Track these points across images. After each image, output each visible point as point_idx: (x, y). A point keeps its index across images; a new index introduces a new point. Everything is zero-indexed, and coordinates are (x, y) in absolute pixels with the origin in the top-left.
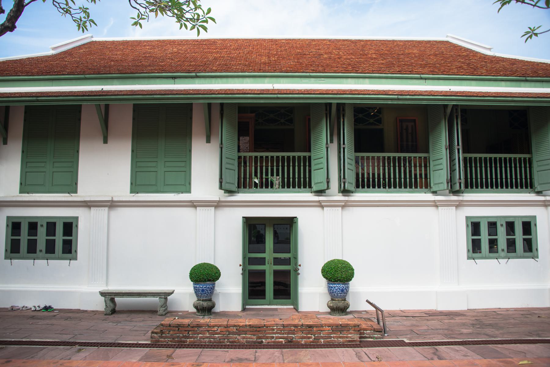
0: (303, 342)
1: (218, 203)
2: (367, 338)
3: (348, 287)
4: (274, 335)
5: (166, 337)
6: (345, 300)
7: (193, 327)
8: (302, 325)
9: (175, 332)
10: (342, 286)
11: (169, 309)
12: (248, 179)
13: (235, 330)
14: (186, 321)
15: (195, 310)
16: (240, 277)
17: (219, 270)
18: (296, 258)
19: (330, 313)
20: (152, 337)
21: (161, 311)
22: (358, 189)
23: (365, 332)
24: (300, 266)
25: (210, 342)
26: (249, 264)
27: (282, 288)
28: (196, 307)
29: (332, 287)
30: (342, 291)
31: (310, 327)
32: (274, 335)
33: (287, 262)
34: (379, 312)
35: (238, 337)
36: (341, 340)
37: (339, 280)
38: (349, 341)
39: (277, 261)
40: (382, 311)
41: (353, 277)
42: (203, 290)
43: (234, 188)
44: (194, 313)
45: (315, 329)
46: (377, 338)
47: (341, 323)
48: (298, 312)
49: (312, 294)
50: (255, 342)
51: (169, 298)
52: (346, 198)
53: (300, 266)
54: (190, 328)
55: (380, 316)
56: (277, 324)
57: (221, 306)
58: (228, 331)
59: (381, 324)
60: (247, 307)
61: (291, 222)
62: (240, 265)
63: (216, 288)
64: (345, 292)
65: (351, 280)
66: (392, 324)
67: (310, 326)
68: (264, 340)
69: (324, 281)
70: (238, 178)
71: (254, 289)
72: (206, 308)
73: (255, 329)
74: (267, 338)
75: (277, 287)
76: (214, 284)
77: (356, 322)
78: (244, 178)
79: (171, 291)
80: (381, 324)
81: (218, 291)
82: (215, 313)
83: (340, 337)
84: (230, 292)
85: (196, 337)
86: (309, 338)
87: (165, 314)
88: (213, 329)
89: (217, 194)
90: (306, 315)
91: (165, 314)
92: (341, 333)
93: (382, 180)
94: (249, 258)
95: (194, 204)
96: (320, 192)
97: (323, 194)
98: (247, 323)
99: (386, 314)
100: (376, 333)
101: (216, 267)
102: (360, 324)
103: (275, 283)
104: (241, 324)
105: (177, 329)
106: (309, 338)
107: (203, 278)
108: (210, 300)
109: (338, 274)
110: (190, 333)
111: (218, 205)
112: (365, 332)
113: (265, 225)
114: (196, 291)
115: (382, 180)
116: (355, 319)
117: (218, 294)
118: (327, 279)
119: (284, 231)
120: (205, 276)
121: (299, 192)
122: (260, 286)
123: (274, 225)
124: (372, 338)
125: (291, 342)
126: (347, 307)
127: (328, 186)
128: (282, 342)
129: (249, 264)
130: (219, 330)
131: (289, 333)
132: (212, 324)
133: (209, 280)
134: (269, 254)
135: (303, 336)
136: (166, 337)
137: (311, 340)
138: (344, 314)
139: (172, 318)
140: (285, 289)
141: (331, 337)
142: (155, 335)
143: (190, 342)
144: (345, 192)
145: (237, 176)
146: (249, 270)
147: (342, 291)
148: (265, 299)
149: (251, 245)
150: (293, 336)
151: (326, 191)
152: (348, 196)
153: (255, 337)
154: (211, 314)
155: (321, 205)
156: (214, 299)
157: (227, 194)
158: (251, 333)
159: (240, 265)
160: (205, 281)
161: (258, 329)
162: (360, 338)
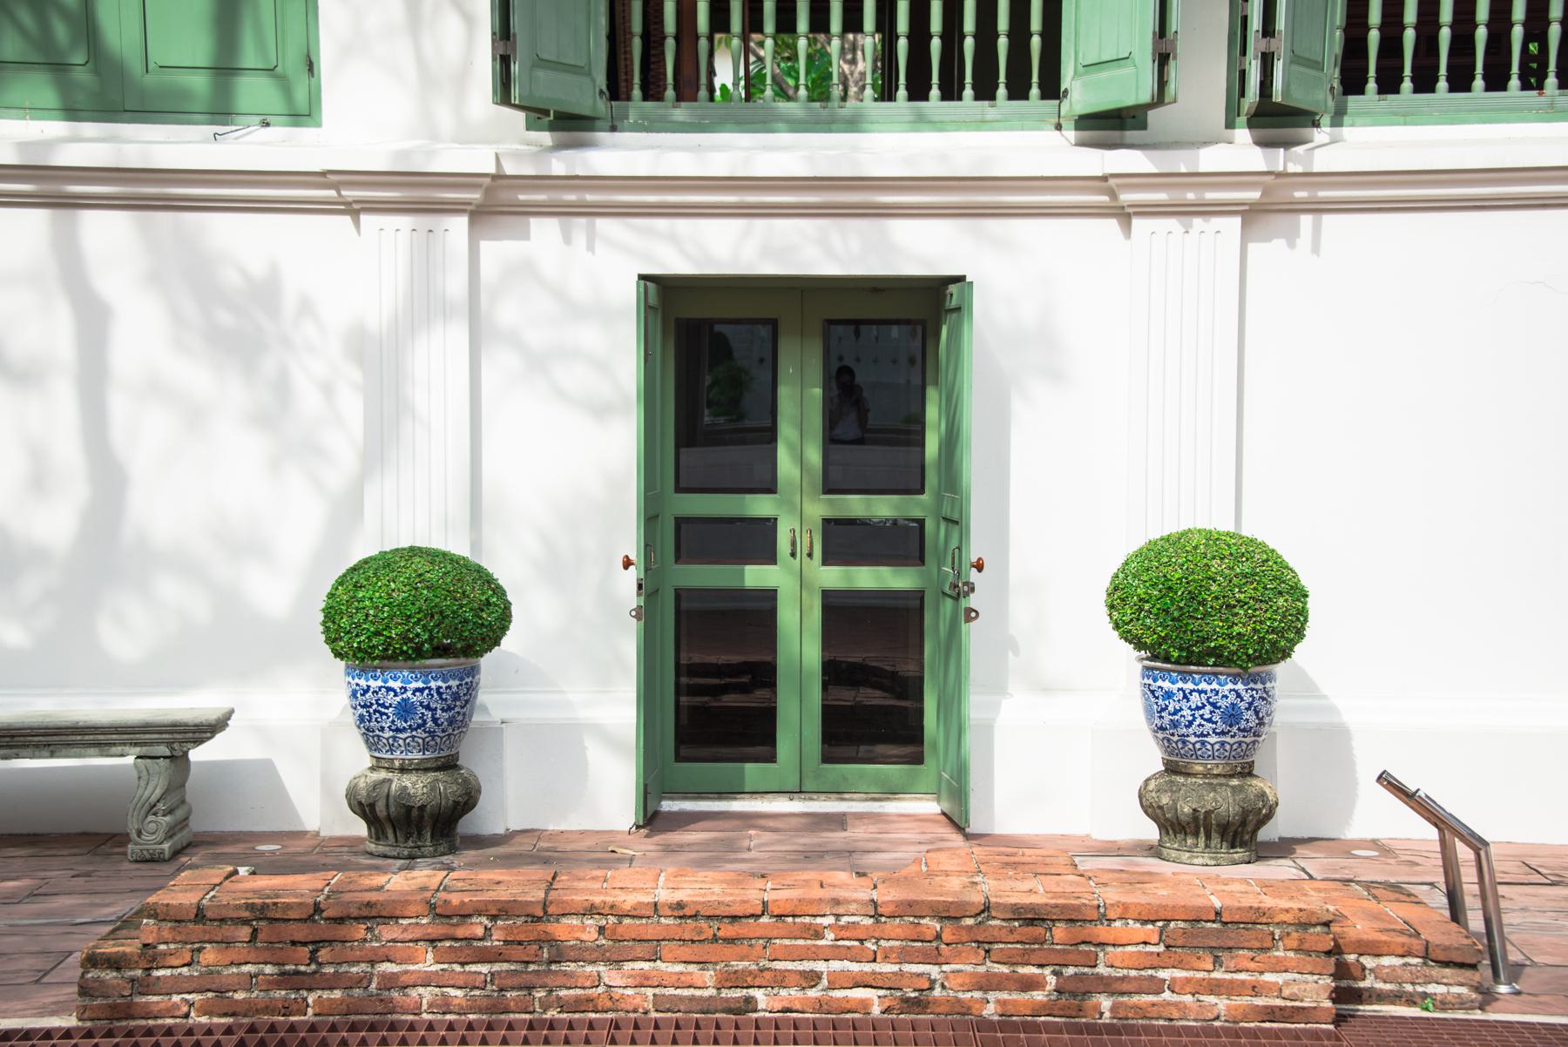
0: (990, 1011)
1: (488, 191)
2: (1381, 997)
3: (1266, 697)
4: (820, 966)
5: (177, 986)
6: (1247, 772)
7: (340, 920)
8: (987, 908)
9: (232, 955)
10: (1226, 689)
11: (198, 824)
12: (670, 44)
13: (590, 935)
14: (301, 887)
15: (360, 828)
16: (627, 645)
17: (499, 591)
18: (956, 522)
19: (1154, 851)
20: (84, 991)
21: (153, 834)
22: (1353, 100)
23: (1368, 962)
24: (979, 567)
25: (445, 1006)
26: (678, 558)
27: (872, 697)
28: (364, 807)
29: (1169, 695)
30: (1232, 716)
31: (1031, 922)
32: (820, 966)
33: (903, 543)
34: (1464, 852)
35: (610, 976)
36: (1221, 1004)
37: (1216, 653)
38: (1271, 1014)
39: (844, 540)
40: (1478, 844)
41: (1300, 634)
42: (405, 709)
43: (587, 94)
44: (351, 843)
45: (1060, 932)
46: (1443, 1005)
47: (1218, 904)
48: (968, 837)
49: (1055, 741)
50: (707, 1006)
51: (197, 755)
52: (1279, 159)
53: (979, 567)
54: (322, 929)
55: (1468, 876)
56: (836, 902)
57: (511, 800)
58: (551, 941)
59: (1476, 922)
60: (668, 806)
61: (930, 304)
62: (627, 563)
63: (483, 697)
64: (1245, 726)
65: (1286, 654)
66: (1542, 928)
67: (1032, 917)
68: (758, 994)
69: (1128, 660)
70: (612, 37)
71: (709, 703)
72: (423, 820)
73: (708, 929)
74: (780, 980)
75: (846, 696)
76: (474, 671)
77: (1315, 901)
78: (646, 37)
79: (212, 717)
80: (1476, 922)
81: (496, 715)
82: (478, 842)
83: (1215, 988)
84: (570, 714)
85: (363, 981)
86: (1029, 984)
87: (176, 853)
88: (461, 932)
89: (491, 139)
90: (1013, 854)
91: (176, 853)
92: (1217, 961)
93: (1517, 32)
94: (680, 522)
95: (350, 194)
96: (1112, 125)
97: (1130, 135)
98: (664, 895)
99: (1502, 867)
100: (1437, 972)
101: (479, 570)
102: (1339, 917)
103: (834, 673)
104: (628, 900)
105: (244, 932)
106: (1029, 984)
107: (404, 638)
108: (449, 765)
109: (1211, 622)
110: (324, 954)
111: (493, 203)
112: (1368, 962)
113: (774, 324)
114: (369, 716)
115: (1517, 32)
116: (1307, 886)
117: (495, 732)
118: (1139, 645)
119: (884, 358)
120: (421, 626)
121: (981, 124)
122: (743, 689)
123: (831, 322)
124: (1410, 1001)
125: (919, 1004)
126: (1261, 812)
127: (1162, 83)
128: (865, 1005)
129: (678, 558)
130: (497, 935)
131: (905, 956)
132: (455, 899)
133: (442, 651)
134: (796, 503)
135: (988, 974)
136: (177, 986)
137: (1039, 996)
138: (1240, 853)
139: (217, 873)
140: (885, 697)
141: (1157, 987)
142: (109, 975)
143: (324, 1009)
144: (1276, 120)
145: (603, 21)
146: (679, 594)
147: (1232, 716)
148: (772, 758)
149: (690, 455)
150: (934, 971)
151: (1152, 115)
152: (1287, 144)
153: (709, 976)
154: (452, 850)
155: (1114, 204)
156: (473, 761)
157: (546, 138)
158: (686, 952)
159: (627, 563)
160: (419, 653)
161: (728, 930)
162: (1339, 996)
